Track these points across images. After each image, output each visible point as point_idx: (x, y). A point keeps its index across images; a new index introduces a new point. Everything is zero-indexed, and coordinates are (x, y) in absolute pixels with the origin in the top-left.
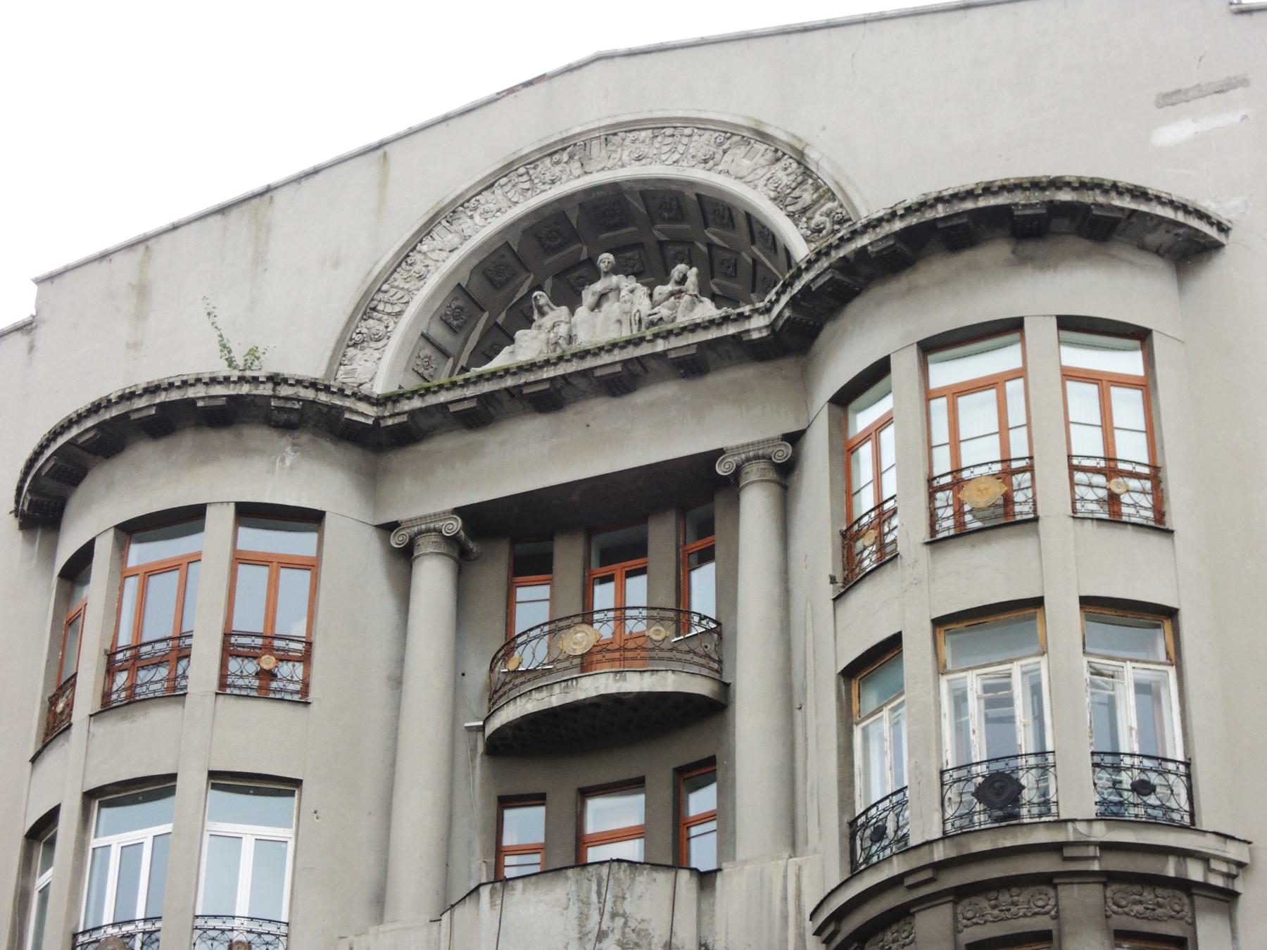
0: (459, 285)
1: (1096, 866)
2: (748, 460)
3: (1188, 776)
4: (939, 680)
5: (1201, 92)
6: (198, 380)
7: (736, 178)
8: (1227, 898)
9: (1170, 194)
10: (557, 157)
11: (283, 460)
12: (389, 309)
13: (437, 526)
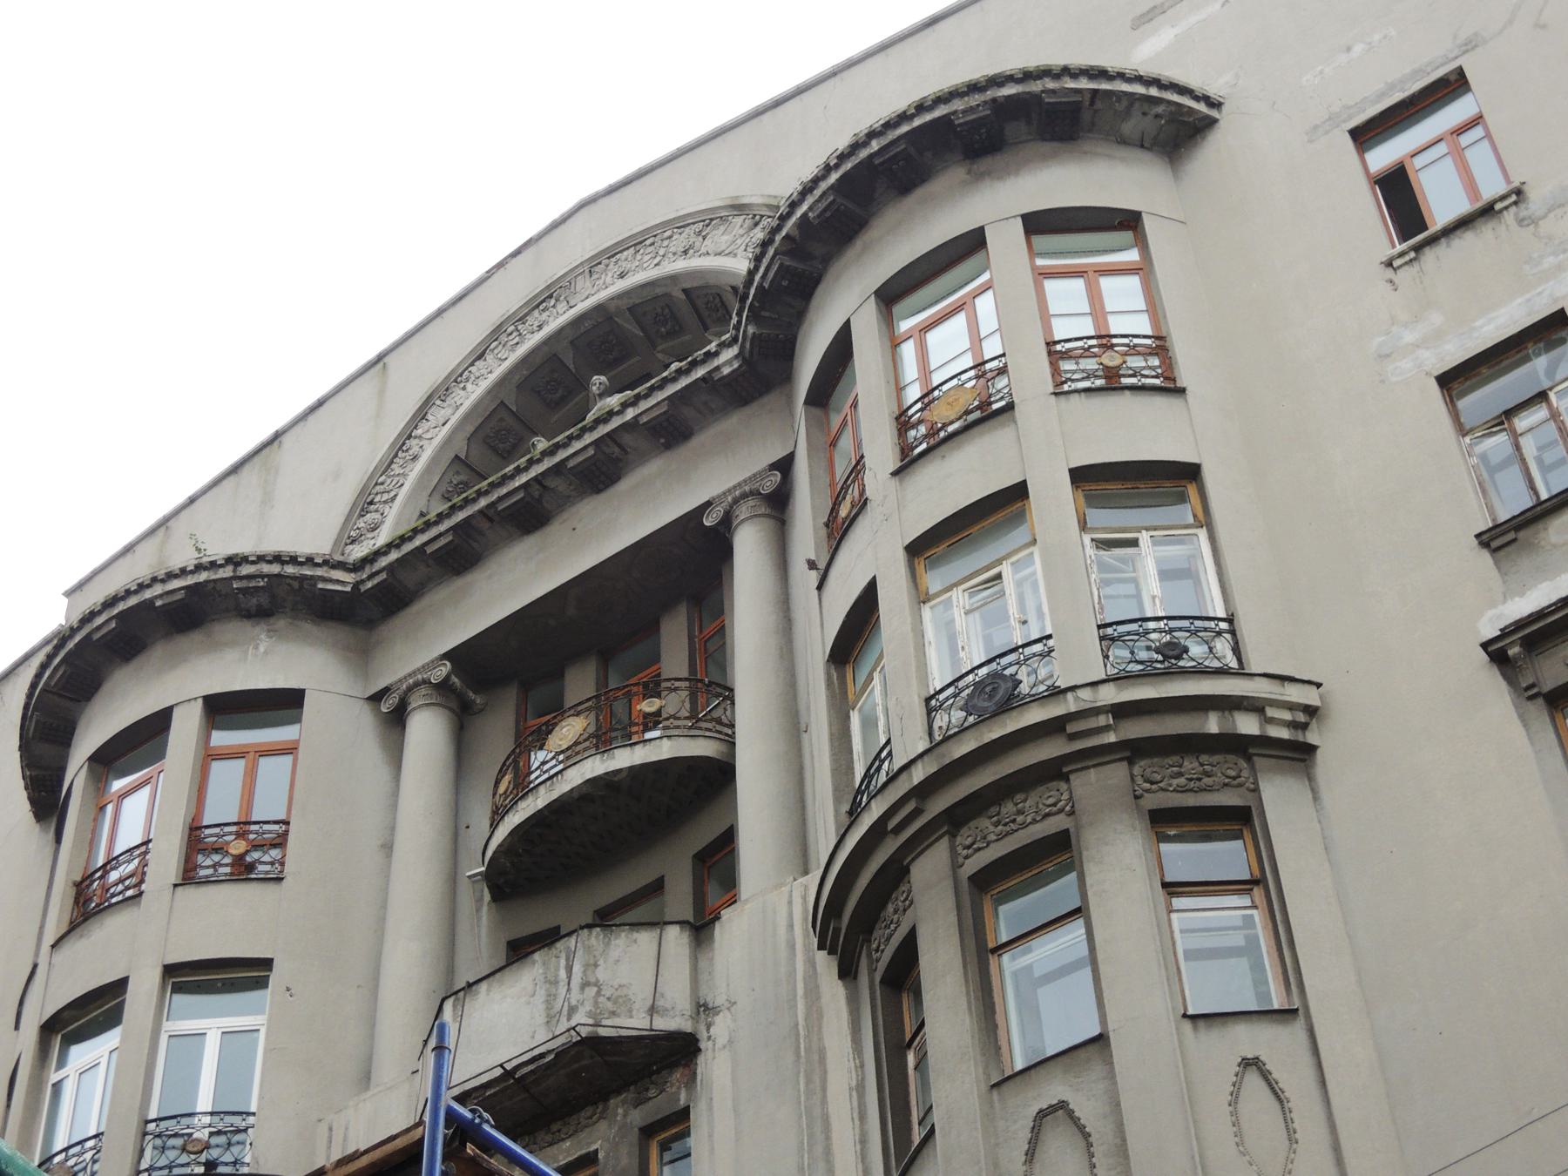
0: (457, 457)
1: (1111, 738)
2: (736, 501)
3: (1233, 632)
4: (920, 609)
7: (715, 255)
8: (1299, 754)
9: (1137, 70)
11: (256, 647)
13: (425, 676)
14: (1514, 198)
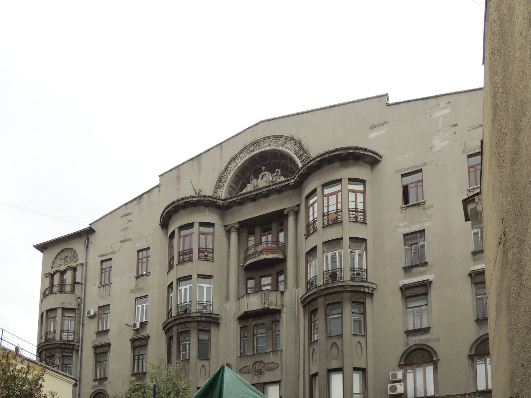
0: (236, 174)
1: (349, 290)
3: (366, 272)
8: (372, 295)
11: (207, 213)
14: (423, 203)
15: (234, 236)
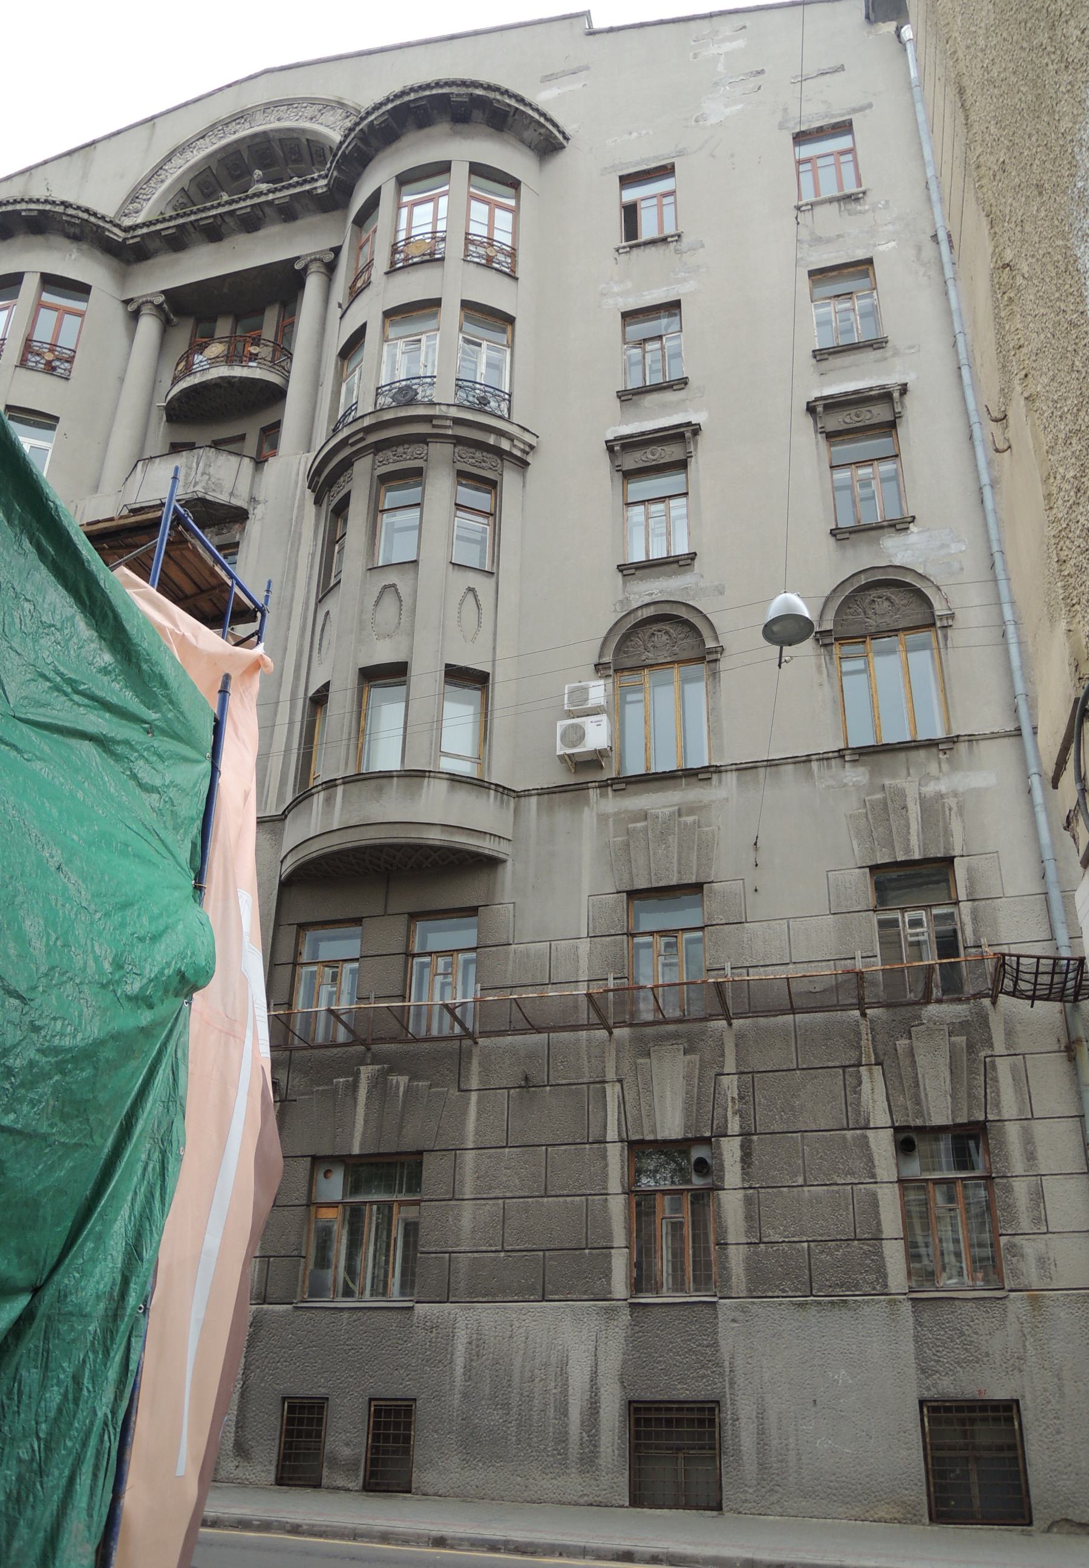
0: (183, 188)
1: (450, 432)
3: (510, 401)
5: (564, 74)
6: (22, 200)
8: (523, 464)
10: (237, 121)
11: (71, 255)
12: (145, 197)
15: (148, 326)
